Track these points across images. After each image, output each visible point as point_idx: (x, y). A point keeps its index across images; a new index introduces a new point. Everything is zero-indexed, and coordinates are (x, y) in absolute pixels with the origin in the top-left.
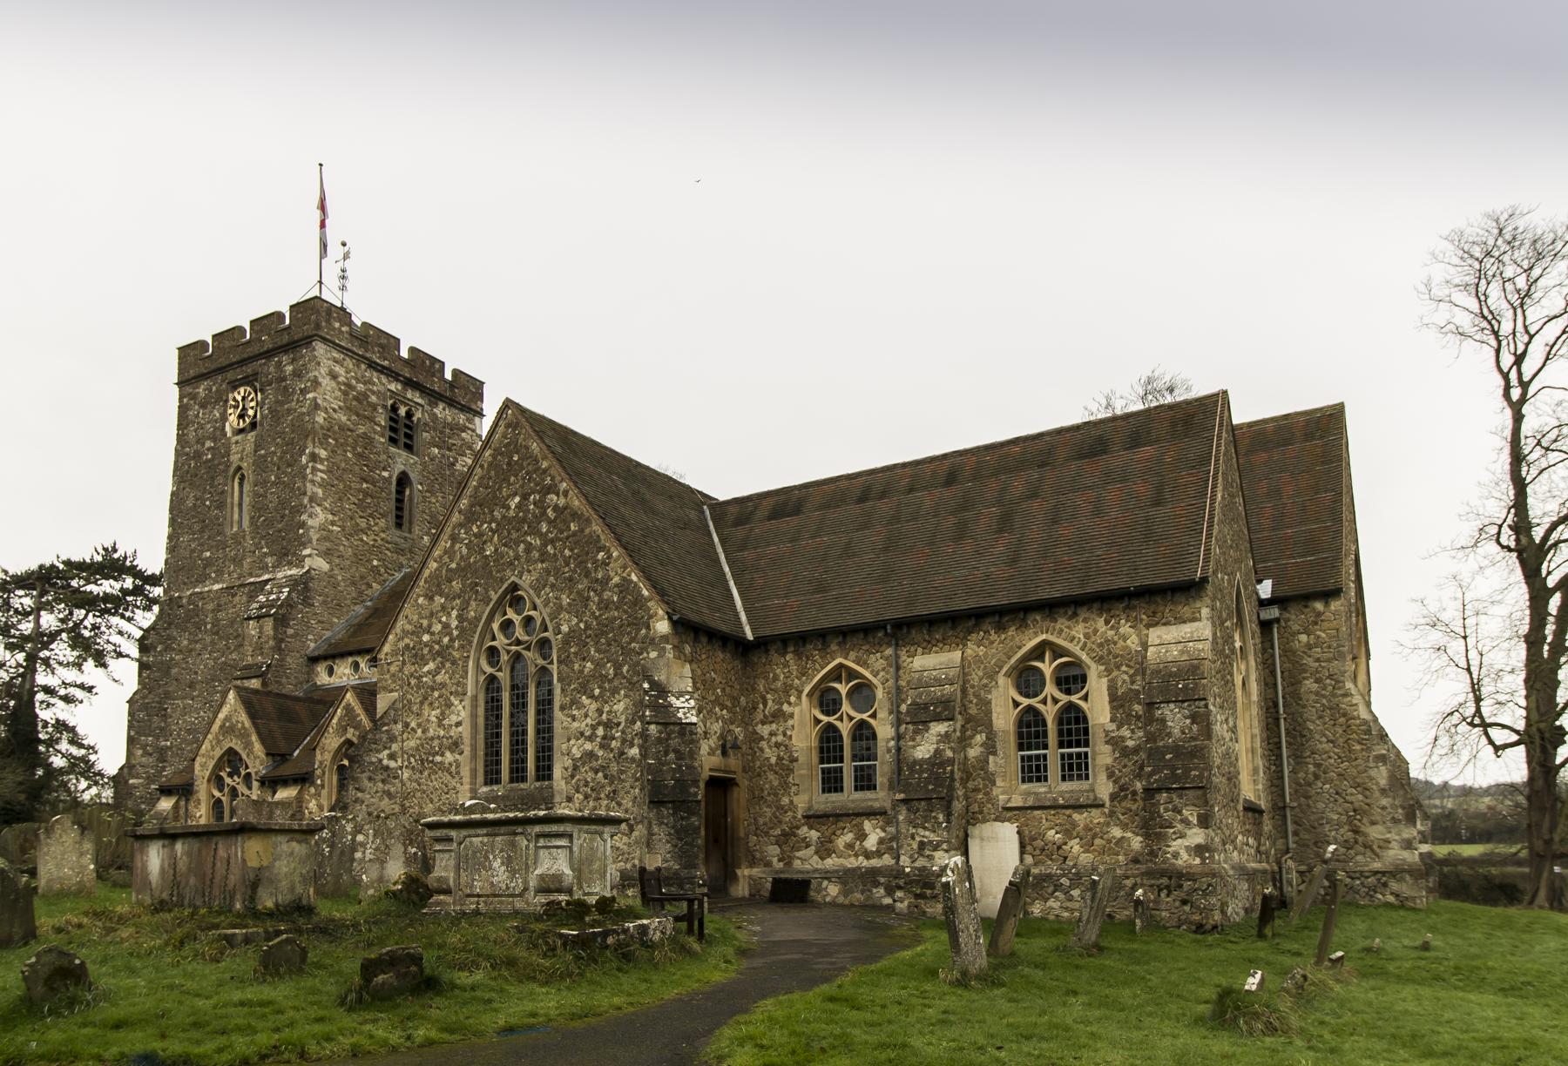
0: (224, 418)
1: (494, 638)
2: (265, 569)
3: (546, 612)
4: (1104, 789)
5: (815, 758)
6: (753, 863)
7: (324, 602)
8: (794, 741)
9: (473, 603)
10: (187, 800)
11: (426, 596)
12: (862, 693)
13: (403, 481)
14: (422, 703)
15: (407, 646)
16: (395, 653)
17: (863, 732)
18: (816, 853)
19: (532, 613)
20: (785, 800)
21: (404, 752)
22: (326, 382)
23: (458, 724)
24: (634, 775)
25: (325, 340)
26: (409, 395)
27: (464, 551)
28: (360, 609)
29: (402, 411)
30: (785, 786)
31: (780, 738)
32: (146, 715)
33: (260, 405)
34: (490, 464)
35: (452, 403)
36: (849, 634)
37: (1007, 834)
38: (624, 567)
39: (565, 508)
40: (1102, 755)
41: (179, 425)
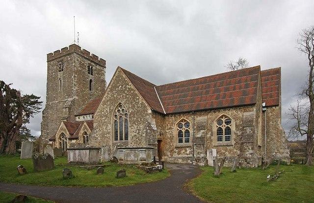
4: (233, 142)
5: (178, 136)
6: (165, 156)
12: (187, 124)
13: (91, 81)
17: (187, 132)
20: (171, 144)
29: (91, 67)
32: (44, 126)
37: (214, 151)
40: (233, 136)
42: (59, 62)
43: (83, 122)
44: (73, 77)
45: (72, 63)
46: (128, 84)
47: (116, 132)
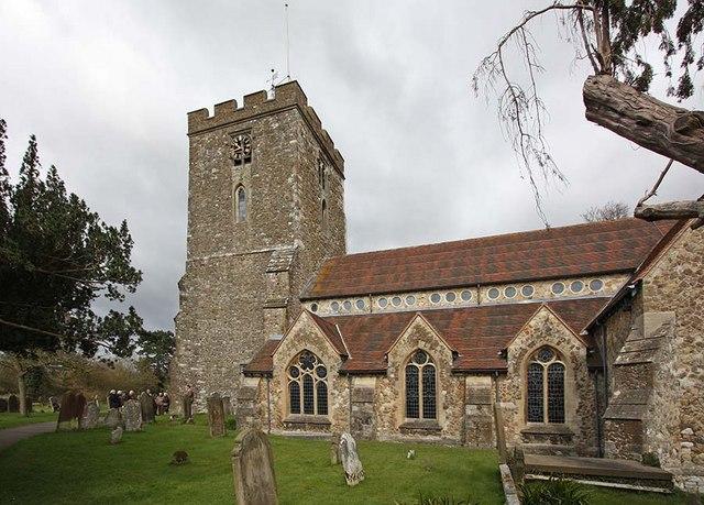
41: (191, 160)
42: (233, 135)
44: (290, 180)
45: (288, 139)
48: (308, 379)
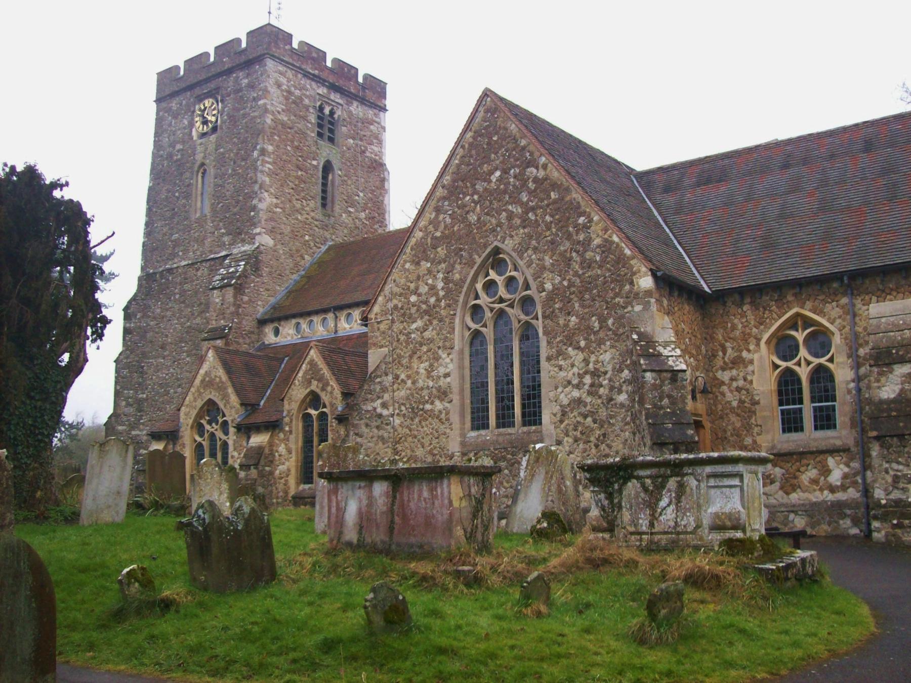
0: (192, 124)
1: (477, 297)
2: (222, 246)
3: (529, 273)
5: (775, 399)
7: (270, 273)
8: (755, 385)
9: (458, 267)
10: (174, 444)
11: (413, 262)
12: (819, 341)
13: (327, 168)
14: (411, 357)
15: (396, 307)
16: (384, 312)
17: (822, 376)
18: (781, 488)
19: (514, 273)
21: (394, 402)
22: (273, 90)
23: (447, 375)
24: (624, 419)
25: (273, 57)
26: (332, 97)
27: (448, 220)
28: (295, 277)
29: (327, 111)
30: (748, 428)
31: (741, 383)
33: (221, 112)
34: (471, 144)
35: (363, 101)
36: (802, 286)
38: (606, 230)
39: (546, 179)
43: (298, 351)
44: (256, 154)
46: (533, 163)
47: (478, 388)
48: (212, 435)
